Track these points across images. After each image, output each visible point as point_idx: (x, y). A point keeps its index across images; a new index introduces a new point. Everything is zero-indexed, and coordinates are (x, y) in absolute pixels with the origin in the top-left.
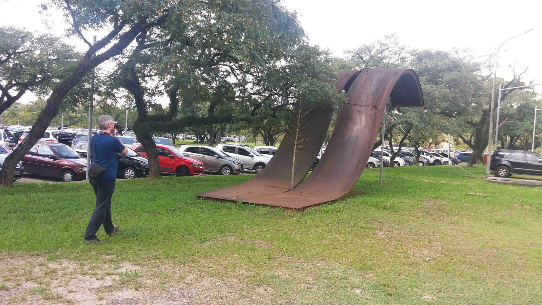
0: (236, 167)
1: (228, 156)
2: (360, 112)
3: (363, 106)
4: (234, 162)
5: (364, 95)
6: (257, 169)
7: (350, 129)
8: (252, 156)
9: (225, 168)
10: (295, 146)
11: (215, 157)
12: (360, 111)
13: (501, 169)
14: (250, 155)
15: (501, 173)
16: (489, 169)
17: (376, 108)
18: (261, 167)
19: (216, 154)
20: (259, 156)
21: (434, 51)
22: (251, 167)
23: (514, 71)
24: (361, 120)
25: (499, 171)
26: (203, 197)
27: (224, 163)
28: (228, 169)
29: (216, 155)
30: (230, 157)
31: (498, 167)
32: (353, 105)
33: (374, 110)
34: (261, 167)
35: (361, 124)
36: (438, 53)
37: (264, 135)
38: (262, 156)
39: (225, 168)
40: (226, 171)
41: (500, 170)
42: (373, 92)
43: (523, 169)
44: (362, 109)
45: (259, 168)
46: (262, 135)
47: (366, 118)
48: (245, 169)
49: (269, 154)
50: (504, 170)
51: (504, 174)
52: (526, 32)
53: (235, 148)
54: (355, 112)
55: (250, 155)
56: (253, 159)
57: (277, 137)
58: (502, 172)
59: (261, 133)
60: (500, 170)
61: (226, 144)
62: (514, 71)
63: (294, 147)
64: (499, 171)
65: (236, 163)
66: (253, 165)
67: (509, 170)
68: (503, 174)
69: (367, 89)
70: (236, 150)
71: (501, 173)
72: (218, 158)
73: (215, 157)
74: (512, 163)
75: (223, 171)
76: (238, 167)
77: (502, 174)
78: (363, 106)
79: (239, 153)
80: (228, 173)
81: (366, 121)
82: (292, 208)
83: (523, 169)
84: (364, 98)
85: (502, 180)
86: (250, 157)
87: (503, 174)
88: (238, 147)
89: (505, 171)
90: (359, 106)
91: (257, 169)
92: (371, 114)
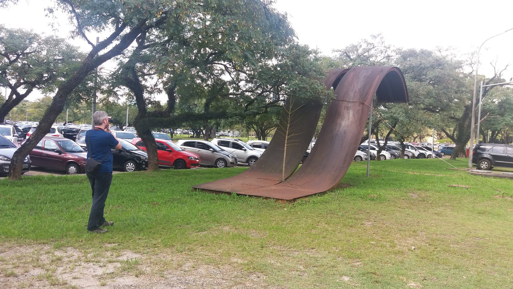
0: (231, 160)
1: (223, 150)
2: (348, 108)
3: (351, 102)
4: (228, 156)
5: (352, 91)
6: (250, 162)
7: (339, 125)
8: (245, 150)
9: (220, 162)
10: (286, 141)
11: (210, 151)
12: (347, 107)
13: (483, 162)
14: (243, 149)
15: (483, 166)
16: (471, 162)
17: (363, 104)
18: (254, 160)
19: (211, 148)
20: (252, 150)
21: (418, 49)
22: (245, 161)
23: (495, 69)
24: (349, 116)
25: (481, 164)
26: (199, 189)
27: (218, 157)
28: (223, 163)
29: (211, 149)
30: (224, 150)
31: (480, 160)
32: (341, 101)
33: (361, 105)
34: (254, 160)
35: (349, 119)
36: (423, 52)
37: (256, 130)
38: (254, 149)
39: (220, 162)
40: (221, 164)
41: (482, 163)
42: (360, 89)
43: (505, 162)
44: (350, 105)
45: (251, 161)
46: (255, 129)
47: (354, 115)
48: (239, 162)
49: (261, 148)
50: (486, 163)
51: (486, 166)
52: (506, 32)
53: (229, 142)
54: (343, 108)
55: (243, 149)
56: (246, 153)
57: (268, 132)
58: (484, 165)
59: (253, 128)
60: (482, 163)
61: (221, 139)
62: (495, 69)
63: (285, 141)
64: (481, 164)
65: (230, 157)
66: (246, 160)
67: (491, 163)
68: (485, 166)
69: (354, 86)
70: (230, 144)
71: (483, 166)
72: (213, 152)
73: (210, 151)
74: (494, 156)
75: (218, 164)
76: (232, 160)
77: (484, 167)
78: (351, 102)
79: (233, 147)
80: (223, 166)
81: (353, 116)
82: (283, 200)
83: (505, 162)
84: (352, 94)
85: (484, 172)
86: (243, 151)
87: (485, 166)
88: (232, 141)
89: (486, 164)
90: (347, 102)
91: (250, 162)
92: (358, 110)
